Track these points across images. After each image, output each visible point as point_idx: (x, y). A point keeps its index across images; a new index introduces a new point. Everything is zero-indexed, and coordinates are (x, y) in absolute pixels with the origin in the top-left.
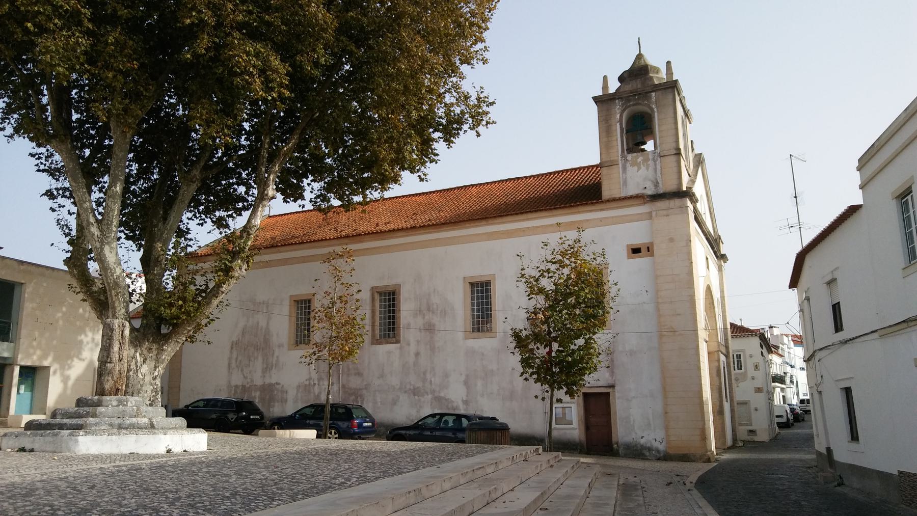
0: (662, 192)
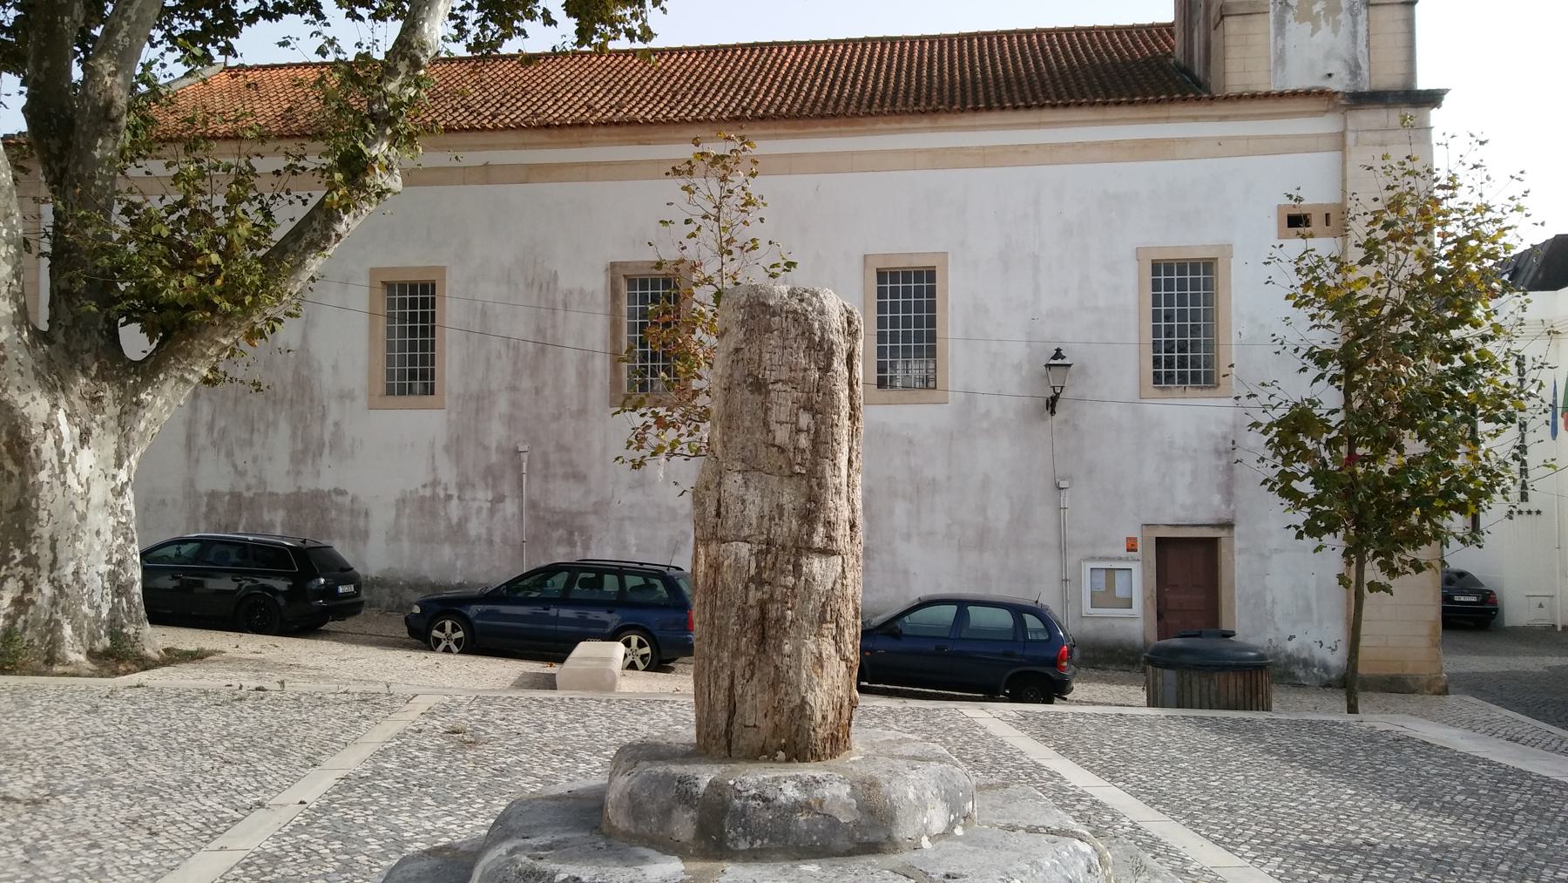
0: (1366, 89)
